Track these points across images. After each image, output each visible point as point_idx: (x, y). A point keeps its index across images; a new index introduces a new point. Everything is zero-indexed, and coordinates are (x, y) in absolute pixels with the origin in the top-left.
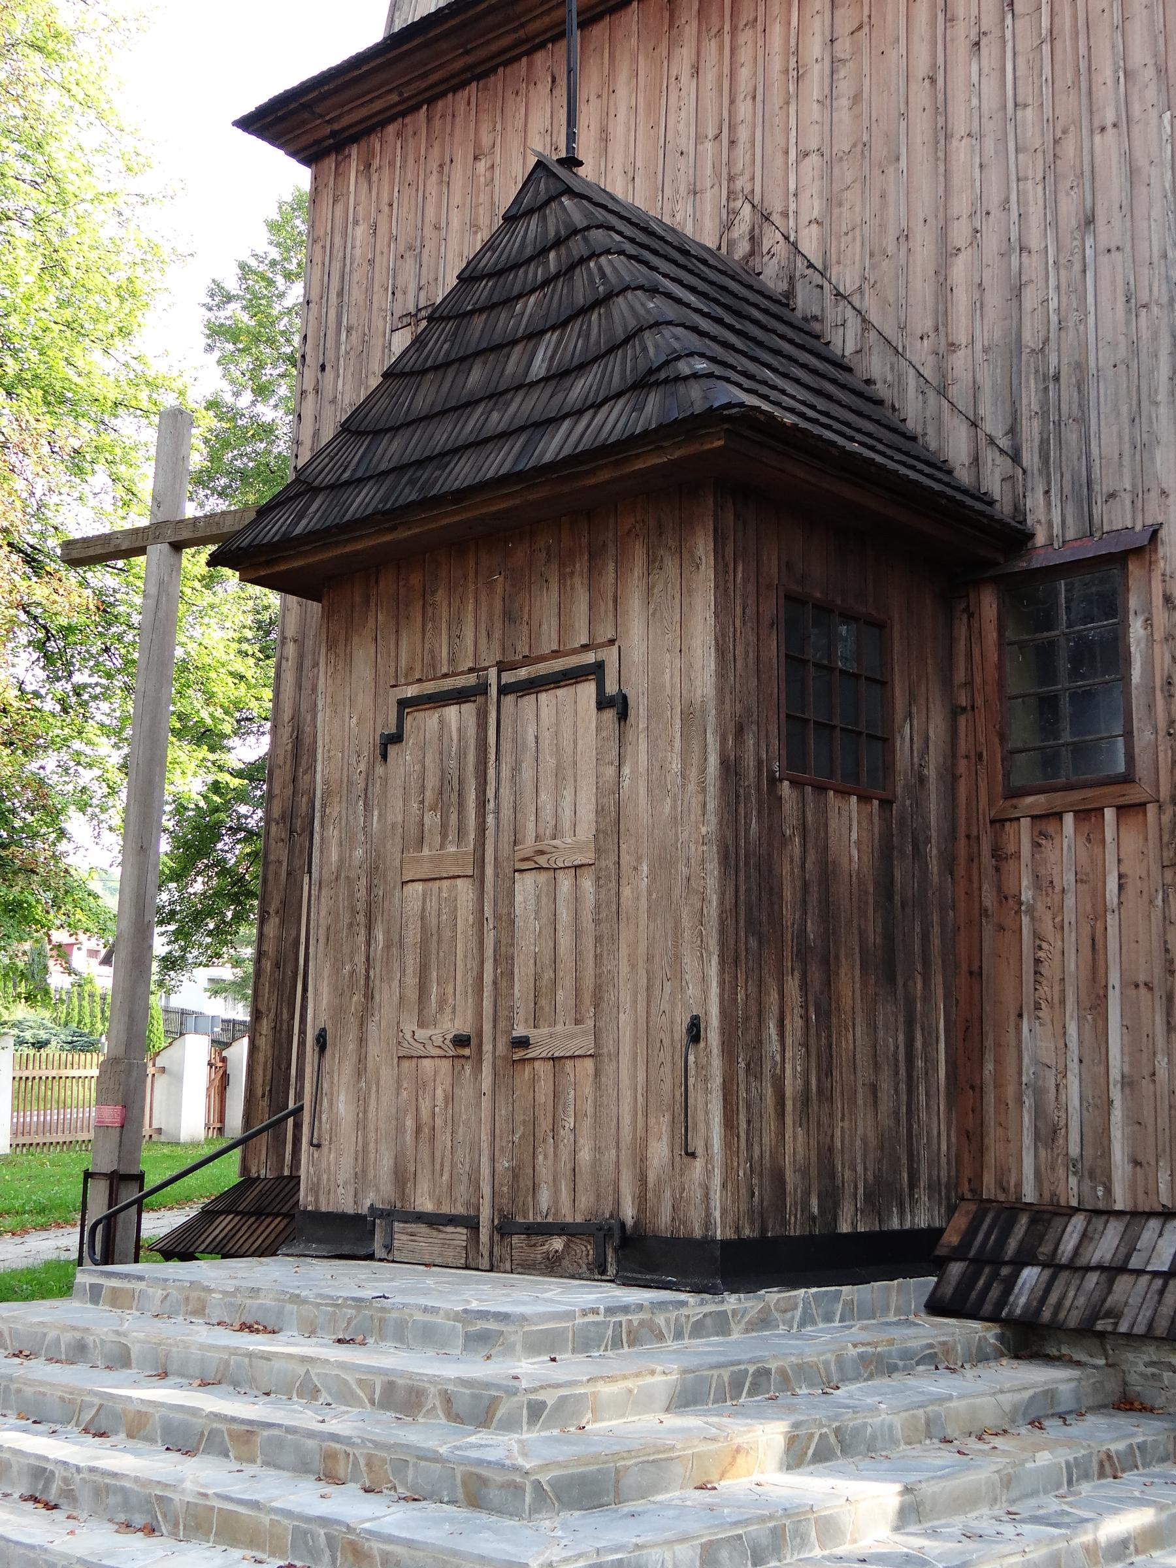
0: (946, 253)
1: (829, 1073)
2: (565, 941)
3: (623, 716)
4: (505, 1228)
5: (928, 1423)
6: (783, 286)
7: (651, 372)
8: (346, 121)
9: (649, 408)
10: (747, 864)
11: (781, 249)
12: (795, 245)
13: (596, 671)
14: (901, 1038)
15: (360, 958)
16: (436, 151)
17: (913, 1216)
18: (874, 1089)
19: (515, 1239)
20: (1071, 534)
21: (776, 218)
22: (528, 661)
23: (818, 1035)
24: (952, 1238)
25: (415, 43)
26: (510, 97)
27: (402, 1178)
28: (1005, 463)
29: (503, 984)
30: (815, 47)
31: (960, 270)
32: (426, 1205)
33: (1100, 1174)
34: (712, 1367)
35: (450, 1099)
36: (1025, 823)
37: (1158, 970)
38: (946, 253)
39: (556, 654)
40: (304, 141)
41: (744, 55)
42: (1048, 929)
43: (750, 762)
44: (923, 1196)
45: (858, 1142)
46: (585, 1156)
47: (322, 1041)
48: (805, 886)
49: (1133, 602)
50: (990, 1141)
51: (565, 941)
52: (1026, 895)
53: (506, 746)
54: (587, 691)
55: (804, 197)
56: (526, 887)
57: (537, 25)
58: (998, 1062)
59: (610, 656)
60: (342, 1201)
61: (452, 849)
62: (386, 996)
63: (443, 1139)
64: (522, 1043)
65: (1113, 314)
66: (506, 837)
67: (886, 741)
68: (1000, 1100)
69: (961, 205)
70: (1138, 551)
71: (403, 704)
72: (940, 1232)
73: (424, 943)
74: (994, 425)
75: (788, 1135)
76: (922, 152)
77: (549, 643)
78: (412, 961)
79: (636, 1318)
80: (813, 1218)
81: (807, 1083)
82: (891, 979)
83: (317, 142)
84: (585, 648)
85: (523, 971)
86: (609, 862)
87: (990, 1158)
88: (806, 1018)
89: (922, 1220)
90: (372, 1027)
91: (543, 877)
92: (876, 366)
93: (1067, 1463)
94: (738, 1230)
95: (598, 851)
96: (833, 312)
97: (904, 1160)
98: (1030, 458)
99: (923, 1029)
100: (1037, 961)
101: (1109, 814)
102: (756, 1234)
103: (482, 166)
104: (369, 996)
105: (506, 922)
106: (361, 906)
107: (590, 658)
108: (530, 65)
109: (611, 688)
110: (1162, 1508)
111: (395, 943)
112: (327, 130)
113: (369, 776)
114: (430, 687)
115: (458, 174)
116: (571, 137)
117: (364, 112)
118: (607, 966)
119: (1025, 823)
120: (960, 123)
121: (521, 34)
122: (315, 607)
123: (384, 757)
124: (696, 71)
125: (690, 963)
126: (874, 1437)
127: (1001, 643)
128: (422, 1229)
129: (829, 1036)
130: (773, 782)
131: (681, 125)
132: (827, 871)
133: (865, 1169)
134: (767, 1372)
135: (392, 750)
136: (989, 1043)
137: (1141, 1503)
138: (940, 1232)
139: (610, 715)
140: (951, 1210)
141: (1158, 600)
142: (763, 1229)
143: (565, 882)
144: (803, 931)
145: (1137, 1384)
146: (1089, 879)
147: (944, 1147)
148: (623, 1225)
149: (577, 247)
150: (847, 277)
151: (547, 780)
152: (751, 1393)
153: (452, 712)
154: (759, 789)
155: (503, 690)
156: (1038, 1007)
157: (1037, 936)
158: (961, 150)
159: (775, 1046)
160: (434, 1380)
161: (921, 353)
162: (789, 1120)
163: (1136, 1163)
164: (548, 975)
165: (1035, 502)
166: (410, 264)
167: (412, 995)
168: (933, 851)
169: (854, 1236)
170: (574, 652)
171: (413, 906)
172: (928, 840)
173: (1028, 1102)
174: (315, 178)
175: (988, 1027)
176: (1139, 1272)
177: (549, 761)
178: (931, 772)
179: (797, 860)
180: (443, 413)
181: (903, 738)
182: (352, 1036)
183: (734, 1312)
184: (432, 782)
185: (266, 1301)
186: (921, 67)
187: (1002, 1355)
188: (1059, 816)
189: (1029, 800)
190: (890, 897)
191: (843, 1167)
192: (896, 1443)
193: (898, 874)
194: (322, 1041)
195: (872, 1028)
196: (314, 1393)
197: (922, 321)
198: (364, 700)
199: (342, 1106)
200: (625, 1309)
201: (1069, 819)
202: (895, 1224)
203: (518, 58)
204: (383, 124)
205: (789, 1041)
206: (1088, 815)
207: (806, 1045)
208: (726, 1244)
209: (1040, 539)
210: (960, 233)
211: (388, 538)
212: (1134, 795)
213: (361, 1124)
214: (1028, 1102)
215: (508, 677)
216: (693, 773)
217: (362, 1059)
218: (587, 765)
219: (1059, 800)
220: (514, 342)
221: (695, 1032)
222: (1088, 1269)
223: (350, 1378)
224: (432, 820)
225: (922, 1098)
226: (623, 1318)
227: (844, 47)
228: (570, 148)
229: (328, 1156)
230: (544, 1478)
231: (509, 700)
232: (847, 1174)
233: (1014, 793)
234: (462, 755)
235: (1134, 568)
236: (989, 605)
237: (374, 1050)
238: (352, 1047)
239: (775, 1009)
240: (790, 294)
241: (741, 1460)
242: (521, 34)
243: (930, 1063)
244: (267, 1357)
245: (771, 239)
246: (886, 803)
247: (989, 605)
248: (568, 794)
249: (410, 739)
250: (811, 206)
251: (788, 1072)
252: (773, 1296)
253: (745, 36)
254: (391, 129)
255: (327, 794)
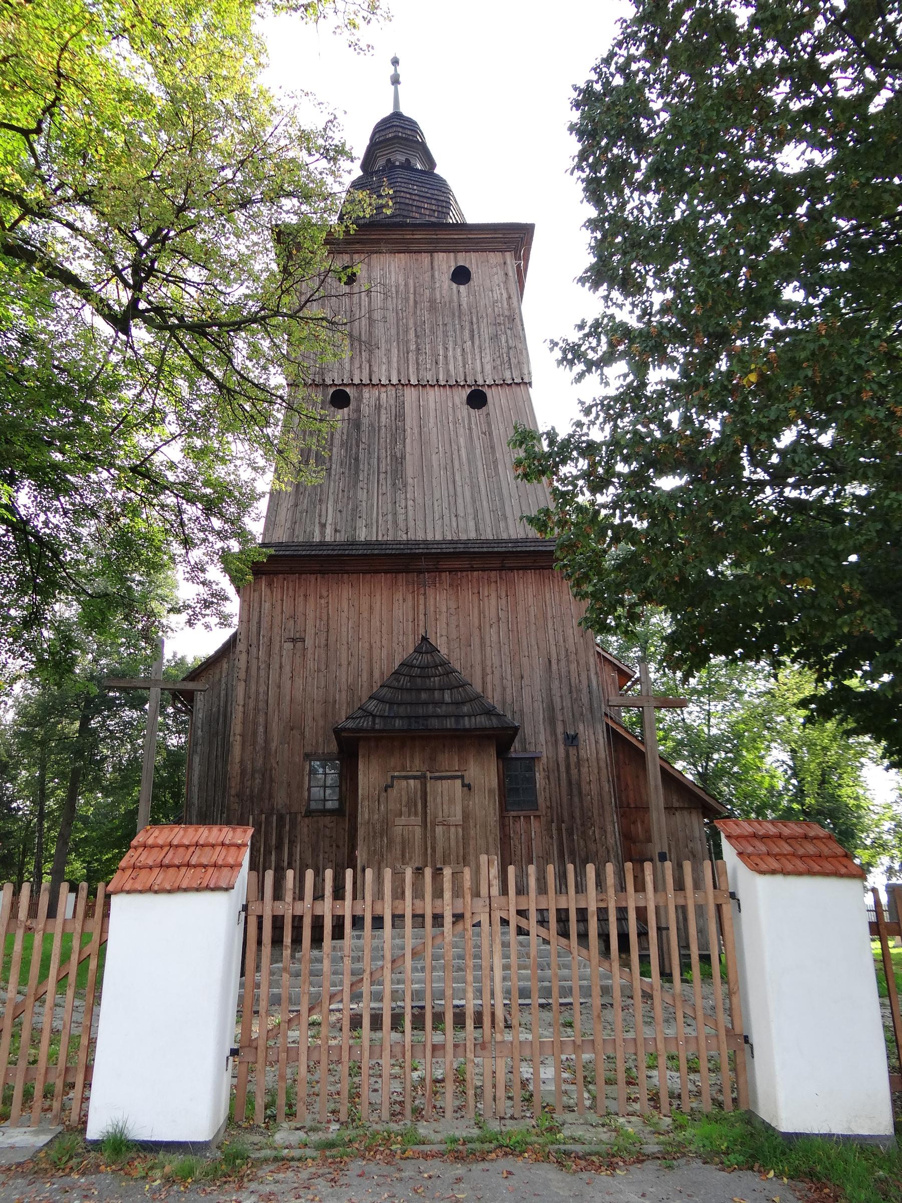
2: (453, 843)
16: (302, 589)
22: (437, 771)
31: (489, 678)
51: (453, 843)
54: (458, 782)
73: (403, 842)
78: (399, 847)
105: (434, 838)
109: (466, 782)
114: (403, 774)
115: (311, 600)
131: (398, 613)
135: (389, 790)
143: (453, 829)
146: (528, 833)
153: (412, 782)
166: (292, 622)
177: (446, 798)
210: (489, 670)
212: (538, 813)
219: (520, 813)
234: (416, 793)
255: (363, 799)
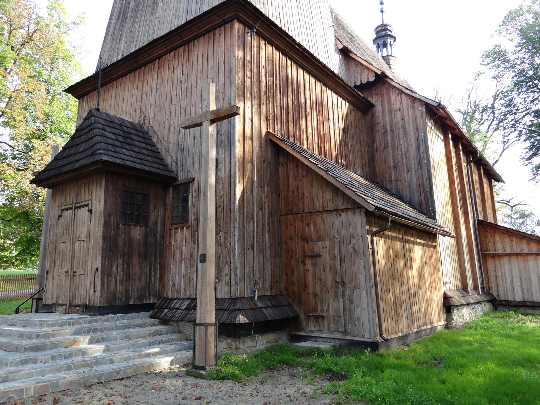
0: (170, 126)
1: (129, 276)
3: (91, 213)
4: (71, 306)
5: (126, 336)
6: (147, 130)
7: (93, 152)
8: (83, 91)
9: (91, 159)
10: (110, 239)
11: (147, 123)
12: (149, 122)
13: (88, 205)
14: (148, 269)
15: (54, 257)
17: (149, 301)
18: (140, 279)
19: (72, 308)
20: (183, 178)
21: (147, 117)
22: (80, 202)
23: (127, 269)
24: (157, 305)
25: (143, 61)
26: (110, 89)
27: (58, 298)
28: (175, 164)
29: (73, 262)
30: (154, 86)
31: (172, 129)
32: (61, 302)
33: (179, 292)
34: (83, 328)
35: (65, 283)
36: (174, 230)
37: (189, 256)
38: (170, 126)
39: (84, 201)
40: (77, 95)
41: (145, 86)
42: (176, 249)
43: (112, 221)
44: (152, 297)
45: (136, 288)
46: (82, 292)
47: (47, 273)
48: (125, 243)
49: (190, 191)
50: (165, 287)
52: (173, 243)
53: (75, 218)
54: (87, 208)
55: (151, 113)
56: (77, 243)
57: (114, 76)
58: (168, 273)
59: (90, 202)
60: (49, 302)
61: (67, 237)
62: (57, 264)
63: (64, 290)
64: (75, 272)
65: (192, 139)
66: (74, 235)
67: (148, 216)
68: (167, 279)
69: (173, 117)
70: (191, 182)
71: (62, 210)
72: (156, 303)
74: (174, 158)
75: (118, 287)
76: (168, 106)
77: (82, 200)
79: (74, 321)
80: (123, 302)
81: (123, 278)
82: (146, 258)
83: (79, 95)
84: (87, 200)
85: (76, 259)
86: (88, 240)
87: (165, 290)
88: (123, 266)
89: (151, 302)
90: (55, 270)
91: (79, 242)
92: (159, 146)
93: (150, 342)
94: (104, 304)
95: (87, 237)
96: (154, 135)
97: (147, 291)
98: (179, 164)
99: (154, 267)
100: (174, 255)
101: (185, 228)
102: (109, 305)
103: (105, 102)
104: (55, 264)
106: (54, 247)
107: (87, 202)
108: (113, 83)
109: (90, 208)
110: (161, 348)
111: (59, 254)
112: (80, 93)
113: (57, 223)
114: (66, 207)
116: (98, 105)
117: (86, 90)
118: (87, 258)
119: (174, 230)
120: (174, 102)
121: (111, 78)
122: (51, 190)
123: (59, 219)
124: (137, 88)
125: (97, 257)
126: (111, 339)
127: (173, 198)
128: (60, 306)
129: (129, 269)
130: (118, 225)
132: (130, 240)
133: (137, 293)
134: (97, 329)
135: (60, 218)
136: (167, 269)
137: (158, 348)
138: (156, 303)
139: (89, 213)
140: (159, 300)
141: (194, 191)
142: (110, 304)
144: (124, 251)
145: (182, 329)
147: (158, 288)
148: (86, 305)
149: (91, 127)
150: (156, 129)
151: (81, 224)
152: (92, 332)
153: (69, 211)
154: (114, 226)
155: (76, 208)
156: (173, 263)
157: (174, 250)
158: (173, 106)
159: (115, 272)
160: (25, 332)
161: (165, 143)
162: (118, 285)
163: (185, 290)
164: (79, 260)
165: (179, 172)
167: (61, 264)
168: (159, 235)
169: (134, 305)
170: (86, 201)
171: (62, 247)
172: (158, 233)
173: (171, 279)
174: (79, 102)
175: (167, 266)
176: (181, 309)
178: (159, 221)
179: (123, 238)
180: (67, 157)
181: (152, 215)
182: (52, 271)
183: (99, 319)
184: (65, 224)
185: (15, 321)
186: (169, 91)
187: (159, 325)
188: (178, 228)
189: (174, 226)
190: (147, 244)
191: (132, 292)
192: (118, 340)
193: (149, 240)
194: (47, 273)
195: (141, 267)
196: (10, 335)
197: (166, 138)
198: (57, 209)
199: (50, 285)
200: (72, 319)
201: (179, 229)
202: (145, 302)
203: (111, 82)
204: (90, 92)
205: (119, 270)
206: (182, 228)
207: (123, 271)
208: (100, 307)
209: (179, 179)
211: (56, 180)
213: (53, 288)
214: (171, 279)
215: (76, 206)
216: (100, 224)
217: (53, 276)
218: (86, 222)
220: (79, 144)
221: (97, 270)
222: (174, 309)
223: (15, 333)
224: (65, 231)
225: (153, 280)
226: (71, 321)
227: (158, 86)
228: (98, 107)
229: (48, 294)
230: (27, 347)
231: (76, 210)
232: (133, 294)
233: (172, 225)
235: (191, 185)
236: (171, 190)
237: (55, 274)
238: (52, 273)
239: (116, 265)
240: (148, 131)
241: (76, 343)
242: (111, 78)
243: (155, 274)
244: (6, 330)
245: (146, 121)
246: (146, 227)
247: (171, 190)
248: (83, 227)
249: (63, 216)
250: (152, 115)
251: (118, 276)
252: (109, 316)
253: (145, 82)
254: (91, 94)
